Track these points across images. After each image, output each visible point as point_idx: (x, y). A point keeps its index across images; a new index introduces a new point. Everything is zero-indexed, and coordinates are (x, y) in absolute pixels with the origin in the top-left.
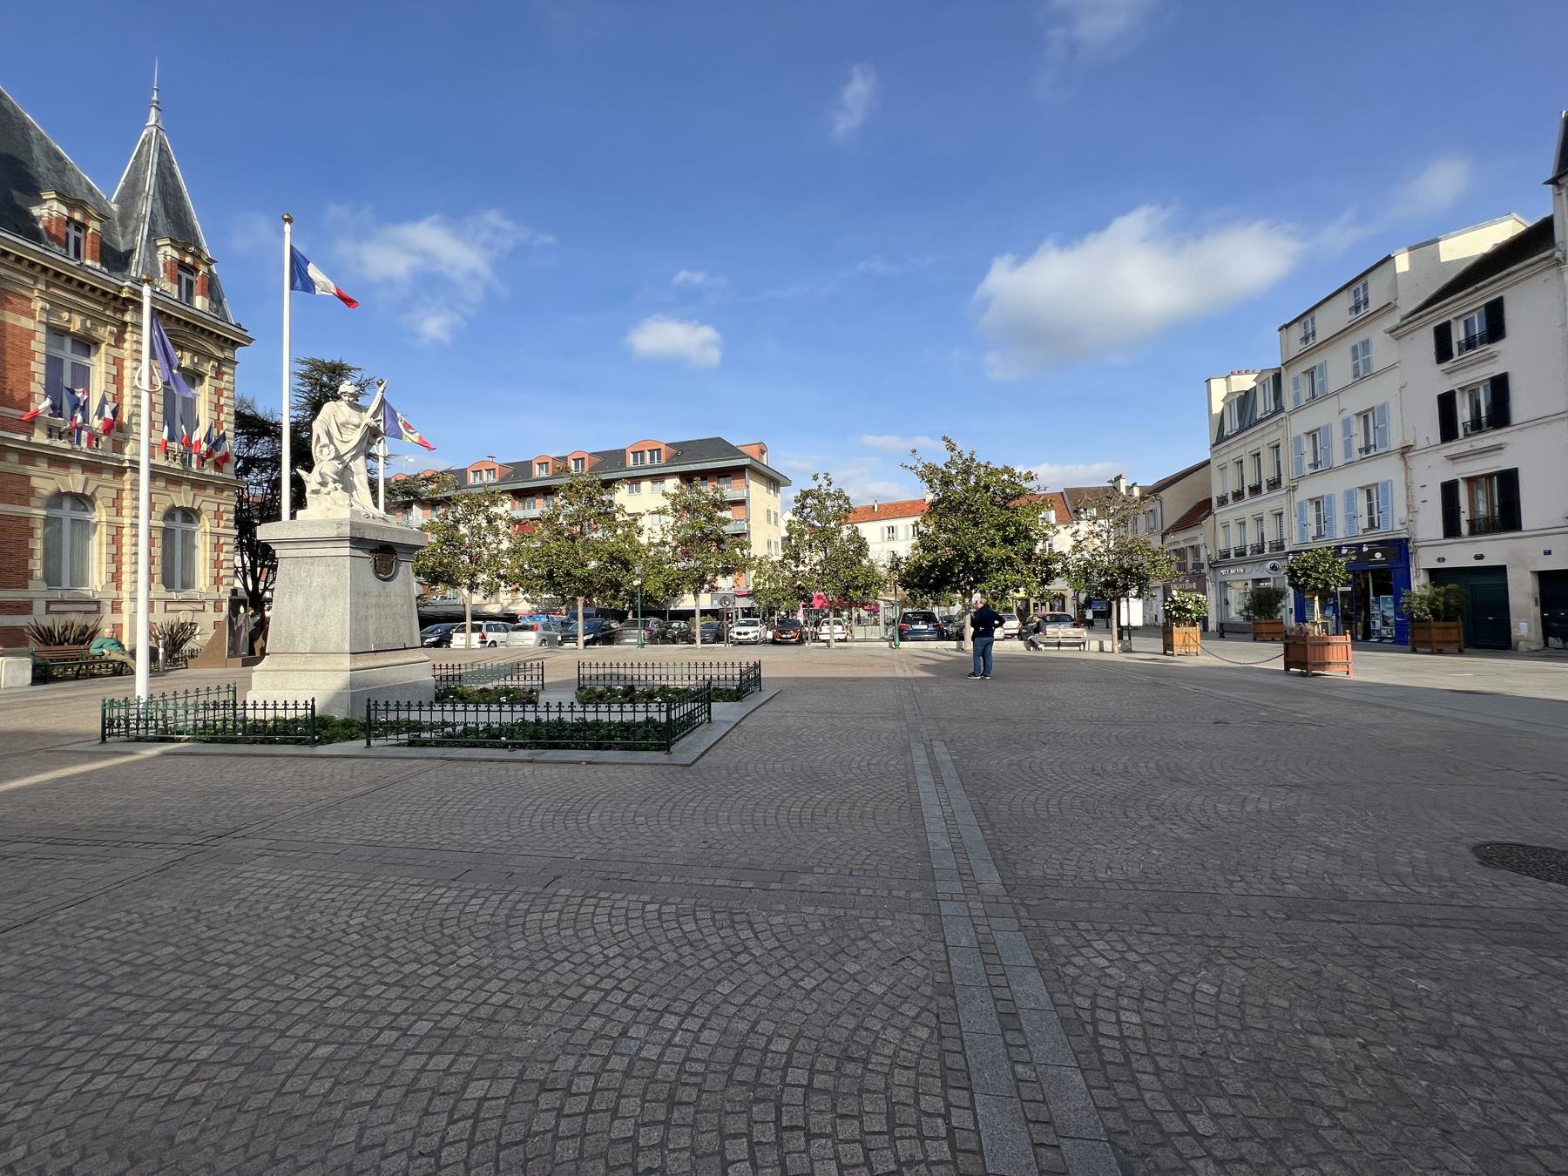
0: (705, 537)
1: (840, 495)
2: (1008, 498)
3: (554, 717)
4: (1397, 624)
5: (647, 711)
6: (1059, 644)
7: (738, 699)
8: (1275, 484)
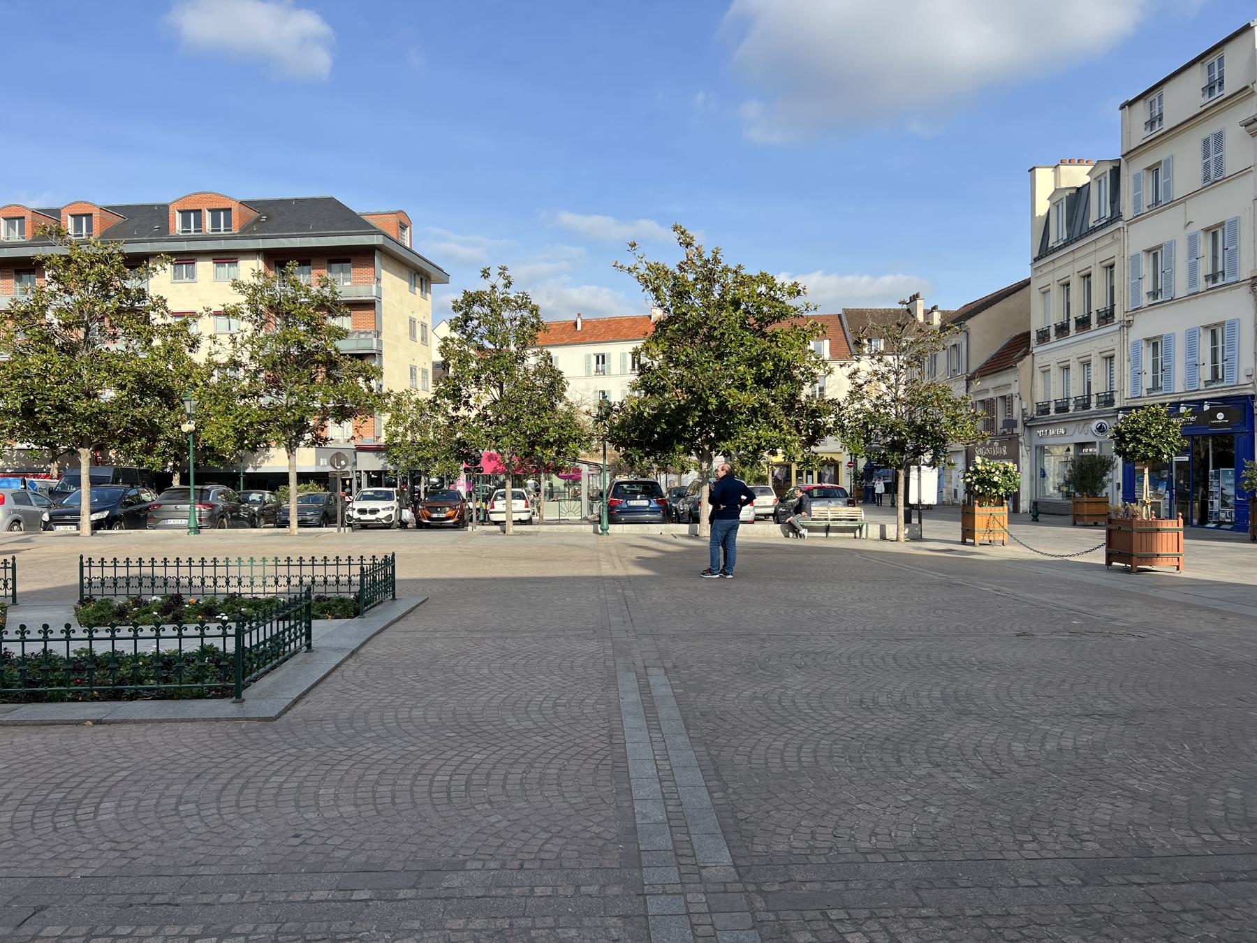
0: (306, 359)
1: (523, 303)
2: (764, 320)
3: (34, 648)
4: (1238, 505)
5: (202, 636)
6: (827, 529)
7: (357, 613)
8: (1107, 317)
